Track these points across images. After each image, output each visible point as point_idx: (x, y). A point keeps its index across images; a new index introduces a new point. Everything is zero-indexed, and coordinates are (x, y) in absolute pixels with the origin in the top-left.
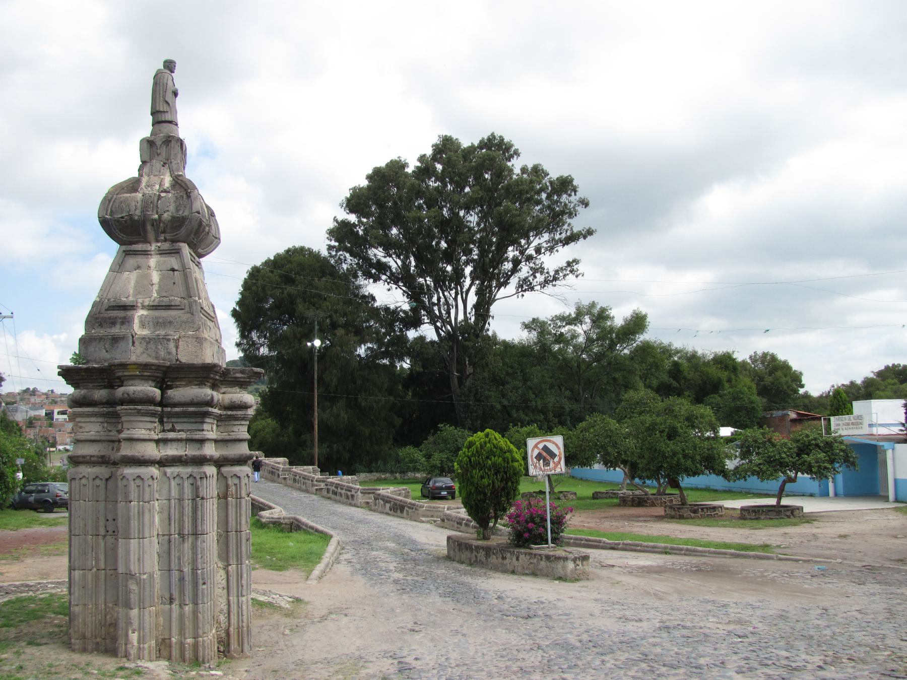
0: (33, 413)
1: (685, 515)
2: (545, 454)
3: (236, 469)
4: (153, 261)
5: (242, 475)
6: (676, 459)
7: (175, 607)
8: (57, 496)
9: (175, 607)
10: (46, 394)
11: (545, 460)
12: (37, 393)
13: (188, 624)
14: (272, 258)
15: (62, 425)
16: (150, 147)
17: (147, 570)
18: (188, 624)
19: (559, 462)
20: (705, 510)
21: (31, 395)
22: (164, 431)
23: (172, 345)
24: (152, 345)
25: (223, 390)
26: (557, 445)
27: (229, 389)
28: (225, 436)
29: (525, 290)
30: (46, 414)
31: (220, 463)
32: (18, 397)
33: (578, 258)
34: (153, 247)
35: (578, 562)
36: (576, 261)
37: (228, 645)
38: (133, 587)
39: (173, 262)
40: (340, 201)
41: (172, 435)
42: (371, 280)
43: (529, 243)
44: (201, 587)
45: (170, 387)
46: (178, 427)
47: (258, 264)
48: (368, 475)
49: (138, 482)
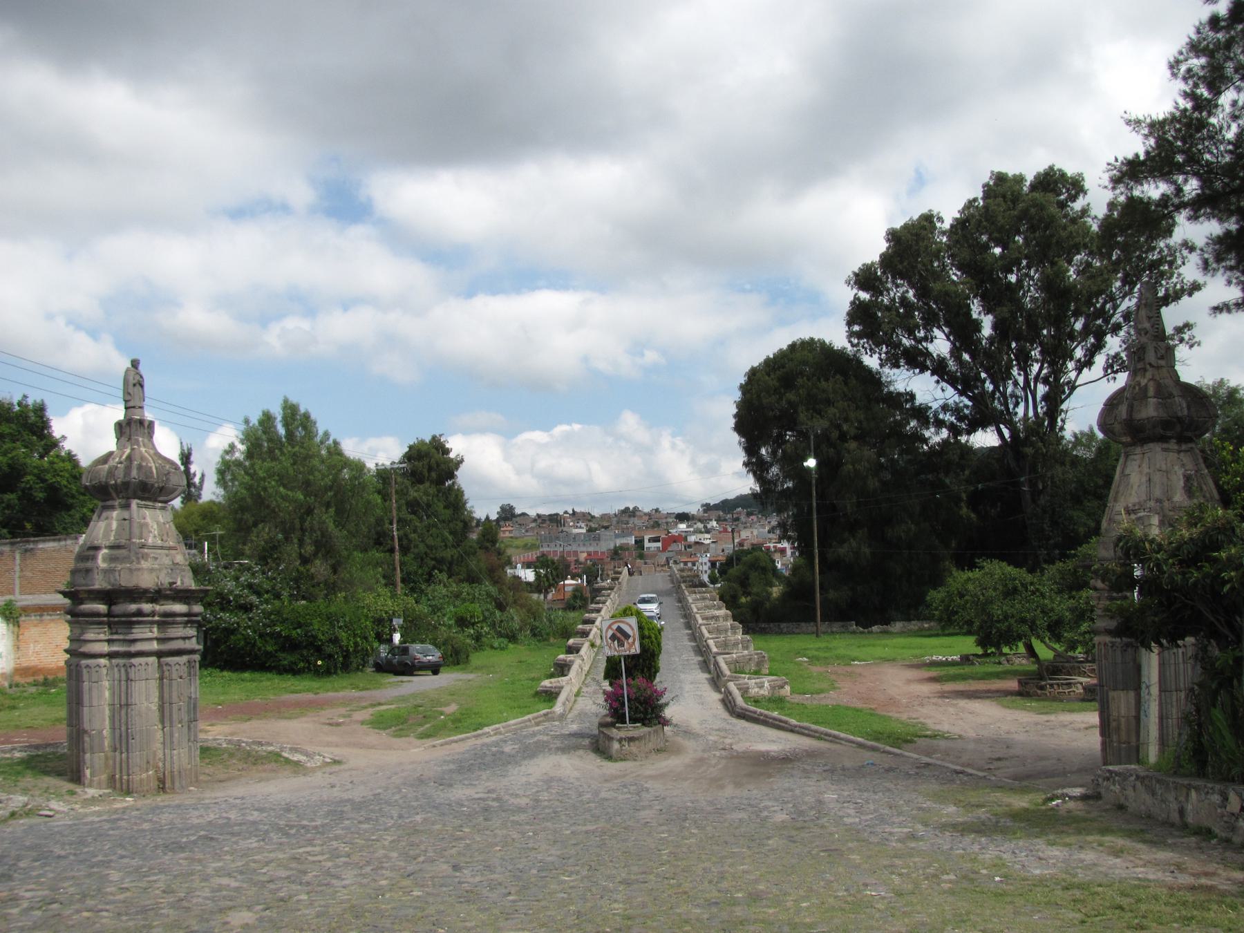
0: (619, 542)
2: (619, 635)
4: (115, 514)
5: (172, 664)
6: (1006, 624)
7: (117, 753)
9: (117, 753)
10: (649, 515)
11: (619, 640)
12: (638, 513)
13: (124, 765)
14: (772, 356)
15: (654, 556)
16: (123, 429)
18: (124, 765)
19: (634, 643)
20: (1055, 686)
21: (630, 516)
22: (112, 634)
23: (117, 574)
26: (630, 626)
28: (162, 636)
29: (1116, 372)
30: (636, 542)
31: (160, 654)
33: (1191, 322)
34: (116, 503)
35: (623, 743)
36: (1188, 326)
38: (87, 739)
39: (126, 514)
40: (845, 277)
41: (115, 637)
43: (1115, 307)
44: (130, 741)
45: (115, 604)
47: (756, 364)
48: (906, 624)
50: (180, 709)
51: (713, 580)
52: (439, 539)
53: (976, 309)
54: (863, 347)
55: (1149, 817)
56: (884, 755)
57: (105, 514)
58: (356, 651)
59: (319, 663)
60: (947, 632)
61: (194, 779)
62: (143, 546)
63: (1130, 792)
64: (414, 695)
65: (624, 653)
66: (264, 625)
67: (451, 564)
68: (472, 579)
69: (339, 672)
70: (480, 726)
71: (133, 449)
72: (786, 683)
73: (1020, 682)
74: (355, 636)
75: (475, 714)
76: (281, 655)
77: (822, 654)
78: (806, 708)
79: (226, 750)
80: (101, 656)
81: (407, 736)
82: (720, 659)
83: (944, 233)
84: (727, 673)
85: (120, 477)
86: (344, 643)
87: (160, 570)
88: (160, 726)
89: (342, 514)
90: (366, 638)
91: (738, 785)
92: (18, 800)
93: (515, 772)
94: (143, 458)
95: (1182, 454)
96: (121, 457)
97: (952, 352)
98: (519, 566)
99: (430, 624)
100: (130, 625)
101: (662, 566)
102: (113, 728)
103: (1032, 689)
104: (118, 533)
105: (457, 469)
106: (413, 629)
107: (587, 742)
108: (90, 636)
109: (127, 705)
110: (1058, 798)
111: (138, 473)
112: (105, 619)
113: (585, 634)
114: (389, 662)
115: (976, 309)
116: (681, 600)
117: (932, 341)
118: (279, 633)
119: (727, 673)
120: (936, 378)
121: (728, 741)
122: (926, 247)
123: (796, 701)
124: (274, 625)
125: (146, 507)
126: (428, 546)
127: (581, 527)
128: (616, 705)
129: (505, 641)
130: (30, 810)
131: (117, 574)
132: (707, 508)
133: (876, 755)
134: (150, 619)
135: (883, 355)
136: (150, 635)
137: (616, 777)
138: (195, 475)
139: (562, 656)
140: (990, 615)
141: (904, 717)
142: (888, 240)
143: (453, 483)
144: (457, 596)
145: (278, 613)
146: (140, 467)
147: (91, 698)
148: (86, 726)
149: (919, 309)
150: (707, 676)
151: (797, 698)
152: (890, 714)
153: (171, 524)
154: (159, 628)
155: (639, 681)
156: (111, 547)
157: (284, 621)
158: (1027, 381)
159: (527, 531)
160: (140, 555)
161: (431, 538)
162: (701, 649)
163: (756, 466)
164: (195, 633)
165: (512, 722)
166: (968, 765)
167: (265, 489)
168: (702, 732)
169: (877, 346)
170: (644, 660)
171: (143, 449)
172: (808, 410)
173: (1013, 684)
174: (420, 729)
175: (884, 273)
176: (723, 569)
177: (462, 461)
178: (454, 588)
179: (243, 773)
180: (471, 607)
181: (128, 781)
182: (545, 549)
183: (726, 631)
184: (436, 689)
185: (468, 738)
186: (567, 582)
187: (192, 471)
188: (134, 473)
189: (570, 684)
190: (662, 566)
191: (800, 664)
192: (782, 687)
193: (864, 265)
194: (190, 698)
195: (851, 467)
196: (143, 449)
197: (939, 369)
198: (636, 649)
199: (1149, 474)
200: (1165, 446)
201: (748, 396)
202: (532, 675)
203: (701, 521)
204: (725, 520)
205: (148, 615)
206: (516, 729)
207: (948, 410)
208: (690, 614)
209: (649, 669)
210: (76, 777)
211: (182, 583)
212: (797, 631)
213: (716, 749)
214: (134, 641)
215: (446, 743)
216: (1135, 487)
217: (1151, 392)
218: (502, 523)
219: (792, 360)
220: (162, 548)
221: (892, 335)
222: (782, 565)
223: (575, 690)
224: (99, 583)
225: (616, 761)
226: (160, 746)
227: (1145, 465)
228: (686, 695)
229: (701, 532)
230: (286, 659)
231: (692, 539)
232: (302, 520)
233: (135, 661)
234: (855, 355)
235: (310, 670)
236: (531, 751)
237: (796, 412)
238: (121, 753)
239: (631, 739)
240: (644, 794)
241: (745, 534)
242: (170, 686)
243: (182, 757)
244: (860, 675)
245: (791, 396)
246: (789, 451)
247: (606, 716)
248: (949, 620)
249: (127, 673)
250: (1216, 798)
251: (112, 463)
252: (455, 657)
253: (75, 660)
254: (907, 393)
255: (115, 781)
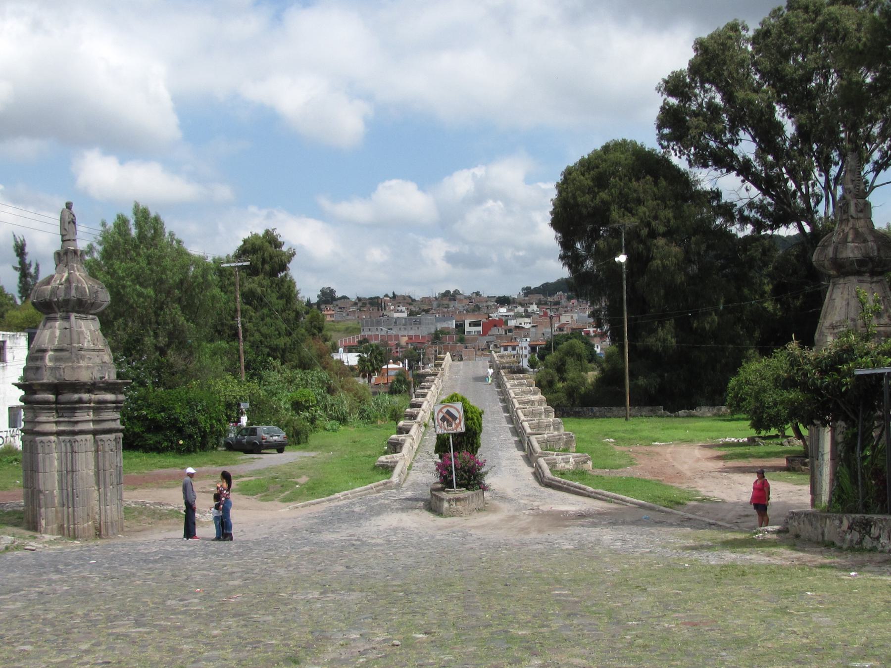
0: (440, 326)
1: (796, 467)
2: (448, 417)
3: (102, 436)
4: (57, 324)
5: (106, 440)
7: (65, 508)
8: (263, 439)
9: (65, 508)
10: (469, 298)
12: (458, 297)
15: (474, 340)
17: (49, 488)
19: (460, 423)
21: (450, 300)
22: (58, 417)
23: (62, 370)
24: (53, 371)
25: (96, 393)
27: (99, 392)
28: (97, 418)
31: (95, 433)
32: (435, 304)
34: (58, 315)
35: (452, 502)
37: (100, 531)
38: (42, 497)
39: (67, 325)
40: (656, 84)
41: (62, 419)
42: (724, 170)
45: (61, 394)
46: (65, 415)
49: (42, 444)
50: (111, 475)
51: (532, 365)
52: (273, 328)
53: (779, 113)
54: (673, 149)
55: (810, 540)
56: (659, 513)
57: (49, 324)
58: (212, 432)
59: (181, 442)
60: (735, 417)
61: (120, 529)
62: (81, 349)
63: (802, 526)
64: (268, 469)
65: (452, 432)
66: (131, 409)
67: (284, 351)
68: (304, 365)
69: (198, 450)
70: (333, 492)
71: (70, 274)
72: (589, 459)
73: (787, 459)
74: (211, 418)
75: (325, 483)
76: (147, 436)
77: (627, 436)
78: (603, 479)
79: (135, 509)
80: (51, 434)
81: (273, 500)
82: (533, 439)
83: (747, 40)
84: (539, 450)
85: (62, 296)
86: (203, 425)
87: (93, 367)
88: (96, 488)
89: (190, 309)
90: (219, 420)
91: (540, 531)
92: (8, 539)
93: (367, 524)
94: (78, 281)
95: (874, 284)
96: (61, 280)
97: (757, 155)
98: (341, 350)
99: (272, 408)
100: (74, 410)
101: (483, 350)
102: (61, 489)
103: (797, 464)
104: (61, 340)
105: (289, 262)
106: (259, 411)
107: (422, 504)
108: (42, 418)
109: (73, 471)
110: (760, 532)
111: (76, 293)
112: (54, 405)
113: (413, 417)
114: (239, 442)
115: (779, 113)
116: (500, 385)
117: (737, 144)
118: (145, 416)
119: (539, 450)
120: (741, 178)
121: (536, 504)
122: (732, 57)
123: (596, 474)
124: (141, 409)
125: (81, 318)
126: (262, 335)
127: (401, 311)
128: (445, 473)
129: (337, 423)
130: (17, 545)
131: (62, 370)
132: (528, 291)
133: (652, 513)
134: (88, 405)
135: (692, 157)
136: (87, 418)
137: (447, 527)
138: (30, 265)
139: (394, 436)
140: (762, 402)
141: (684, 486)
142: (696, 50)
143: (286, 276)
144: (291, 381)
145: (145, 399)
146: (77, 288)
147: (44, 466)
148: (42, 487)
149: (726, 111)
150: (522, 453)
151: (598, 472)
152: (673, 484)
153: (99, 331)
154: (94, 413)
155: (465, 455)
156: (55, 350)
157: (149, 406)
158: (827, 181)
159: (348, 315)
160: (79, 357)
161: (265, 327)
162: (518, 431)
163: (570, 258)
164: (119, 416)
165: (358, 489)
166: (722, 520)
167: (124, 287)
168: (514, 497)
169: (686, 148)
170: (468, 438)
171: (78, 274)
172: (620, 207)
173: (783, 462)
174: (282, 495)
175: (692, 80)
176: (540, 353)
177: (294, 254)
178: (288, 373)
179: (153, 525)
180: (307, 391)
181: (74, 529)
182: (366, 333)
183: (540, 414)
184: (286, 465)
185: (323, 502)
186: (390, 366)
187: (27, 262)
188: (73, 293)
189: (403, 458)
190: (483, 350)
191: (606, 444)
192: (585, 462)
193: (673, 73)
194: (117, 466)
195: (659, 262)
196: (78, 274)
197: (744, 169)
198: (462, 428)
199: (848, 299)
200: (860, 278)
201: (564, 194)
202: (369, 453)
203: (522, 305)
204: (546, 304)
205: (86, 403)
206: (361, 495)
207: (754, 208)
208: (508, 399)
209: (472, 445)
210: (33, 526)
211: (109, 377)
212: (609, 414)
213: (526, 509)
214: (77, 422)
215: (306, 505)
216: (838, 309)
217: (850, 237)
218: (323, 307)
219: (605, 161)
220: (94, 350)
221: (700, 138)
222: (601, 349)
223: (408, 464)
224: (47, 378)
225: (446, 517)
226: (97, 503)
227: (846, 293)
228: (503, 469)
229: (522, 317)
230: (151, 439)
231: (512, 323)
232: (157, 315)
233: (78, 438)
234: (663, 157)
235: (172, 449)
236: (381, 510)
237: (608, 210)
238: (68, 508)
239: (458, 500)
240: (468, 537)
241: (565, 318)
242: (104, 456)
243: (112, 512)
244: (658, 453)
245: (604, 195)
246: (602, 246)
247: (437, 483)
248: (738, 405)
249: (72, 447)
250: (837, 522)
251: (54, 284)
252: (297, 438)
253: (29, 437)
254: (713, 192)
255: (63, 529)
